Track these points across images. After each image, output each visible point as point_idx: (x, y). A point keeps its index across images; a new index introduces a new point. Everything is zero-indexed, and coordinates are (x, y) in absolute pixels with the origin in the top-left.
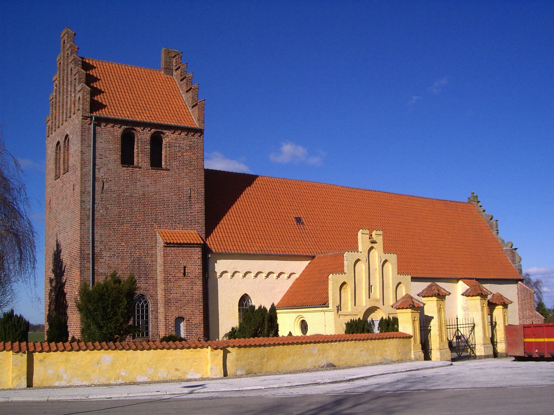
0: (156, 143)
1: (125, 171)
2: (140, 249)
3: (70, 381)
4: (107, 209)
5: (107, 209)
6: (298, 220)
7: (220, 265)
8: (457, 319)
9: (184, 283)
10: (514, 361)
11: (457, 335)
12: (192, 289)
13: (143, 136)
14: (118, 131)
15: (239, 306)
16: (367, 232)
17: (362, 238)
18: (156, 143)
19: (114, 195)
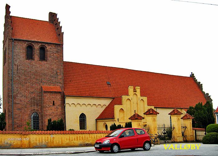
0: (43, 49)
1: (28, 62)
2: (34, 93)
3: (144, 111)
4: (19, 77)
5: (19, 77)
6: (54, 104)
7: (68, 101)
8: (164, 125)
9: (53, 108)
10: (99, 153)
11: (164, 132)
12: (57, 110)
13: (37, 47)
14: (25, 45)
15: (80, 118)
16: (132, 87)
17: (131, 89)
18: (43, 49)
19: (23, 71)
